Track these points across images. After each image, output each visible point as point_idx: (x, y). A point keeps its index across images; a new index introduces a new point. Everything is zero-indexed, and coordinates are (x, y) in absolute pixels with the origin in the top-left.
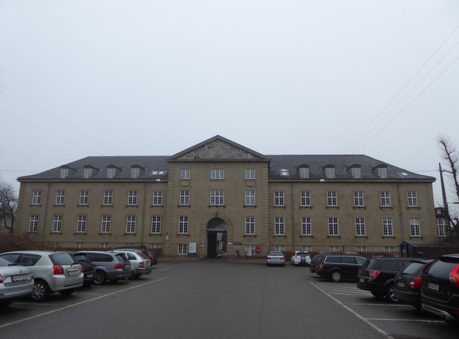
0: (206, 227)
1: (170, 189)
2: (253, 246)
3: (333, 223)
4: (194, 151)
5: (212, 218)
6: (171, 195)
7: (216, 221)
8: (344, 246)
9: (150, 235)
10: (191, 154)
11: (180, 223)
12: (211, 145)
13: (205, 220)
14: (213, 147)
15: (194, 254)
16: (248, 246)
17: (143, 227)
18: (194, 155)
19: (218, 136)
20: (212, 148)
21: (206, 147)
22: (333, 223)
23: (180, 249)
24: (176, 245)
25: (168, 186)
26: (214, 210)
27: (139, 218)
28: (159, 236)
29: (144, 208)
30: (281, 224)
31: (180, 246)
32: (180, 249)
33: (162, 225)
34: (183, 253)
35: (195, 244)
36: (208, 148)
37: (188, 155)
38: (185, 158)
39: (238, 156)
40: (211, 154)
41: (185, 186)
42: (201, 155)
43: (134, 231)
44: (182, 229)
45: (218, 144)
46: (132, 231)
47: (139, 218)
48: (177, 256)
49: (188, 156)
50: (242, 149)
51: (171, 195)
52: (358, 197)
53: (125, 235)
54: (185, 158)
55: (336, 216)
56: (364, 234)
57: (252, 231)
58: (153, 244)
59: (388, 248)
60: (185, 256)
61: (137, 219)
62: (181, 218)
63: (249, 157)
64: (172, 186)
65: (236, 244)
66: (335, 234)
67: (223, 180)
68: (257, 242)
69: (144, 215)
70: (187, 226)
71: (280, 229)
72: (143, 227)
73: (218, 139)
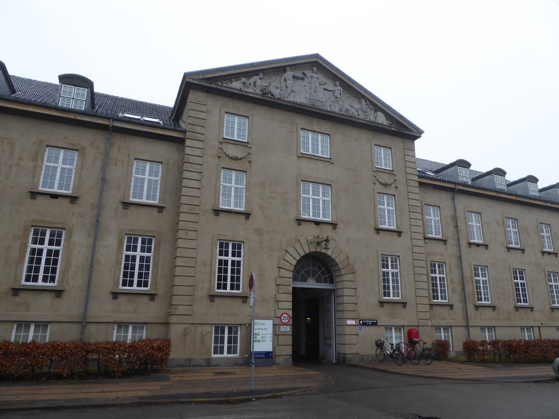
0: (290, 275)
1: (191, 159)
2: (398, 328)
3: (230, 258)
4: (261, 75)
5: (307, 251)
6: (196, 176)
7: (317, 263)
8: (539, 327)
9: (115, 295)
10: (252, 80)
11: (127, 257)
12: (299, 74)
13: (288, 257)
14: (303, 79)
15: (267, 354)
16: (388, 328)
17: (91, 267)
18: (259, 83)
19: (317, 56)
20: (300, 81)
21: (289, 74)
22: (230, 258)
23: (219, 340)
24: (207, 328)
25: (188, 150)
26: (311, 232)
27: (80, 238)
28: (146, 299)
29: (99, 207)
30: (233, 262)
31: (219, 329)
32: (219, 340)
33: (156, 265)
34: (225, 355)
35: (268, 325)
36: (294, 77)
37: (244, 79)
38: (236, 85)
39: (360, 112)
40: (299, 93)
41: (236, 159)
42: (276, 88)
43: (53, 279)
44: (225, 278)
45: (314, 75)
46: (45, 279)
47: (80, 238)
48: (209, 363)
49: (244, 83)
50: (366, 99)
51: (196, 176)
52: (311, 196)
53: (16, 291)
54: (236, 85)
55: (522, 267)
56: (238, 289)
57: (50, 276)
58: (122, 325)
59: (391, 330)
60: (235, 363)
61: (68, 239)
62: (223, 247)
63: (381, 119)
64: (197, 152)
65: (365, 324)
66: (442, 299)
67: (329, 161)
68: (407, 318)
69: (96, 229)
70: (239, 272)
71: (229, 274)
72: (91, 267)
73: (316, 65)
